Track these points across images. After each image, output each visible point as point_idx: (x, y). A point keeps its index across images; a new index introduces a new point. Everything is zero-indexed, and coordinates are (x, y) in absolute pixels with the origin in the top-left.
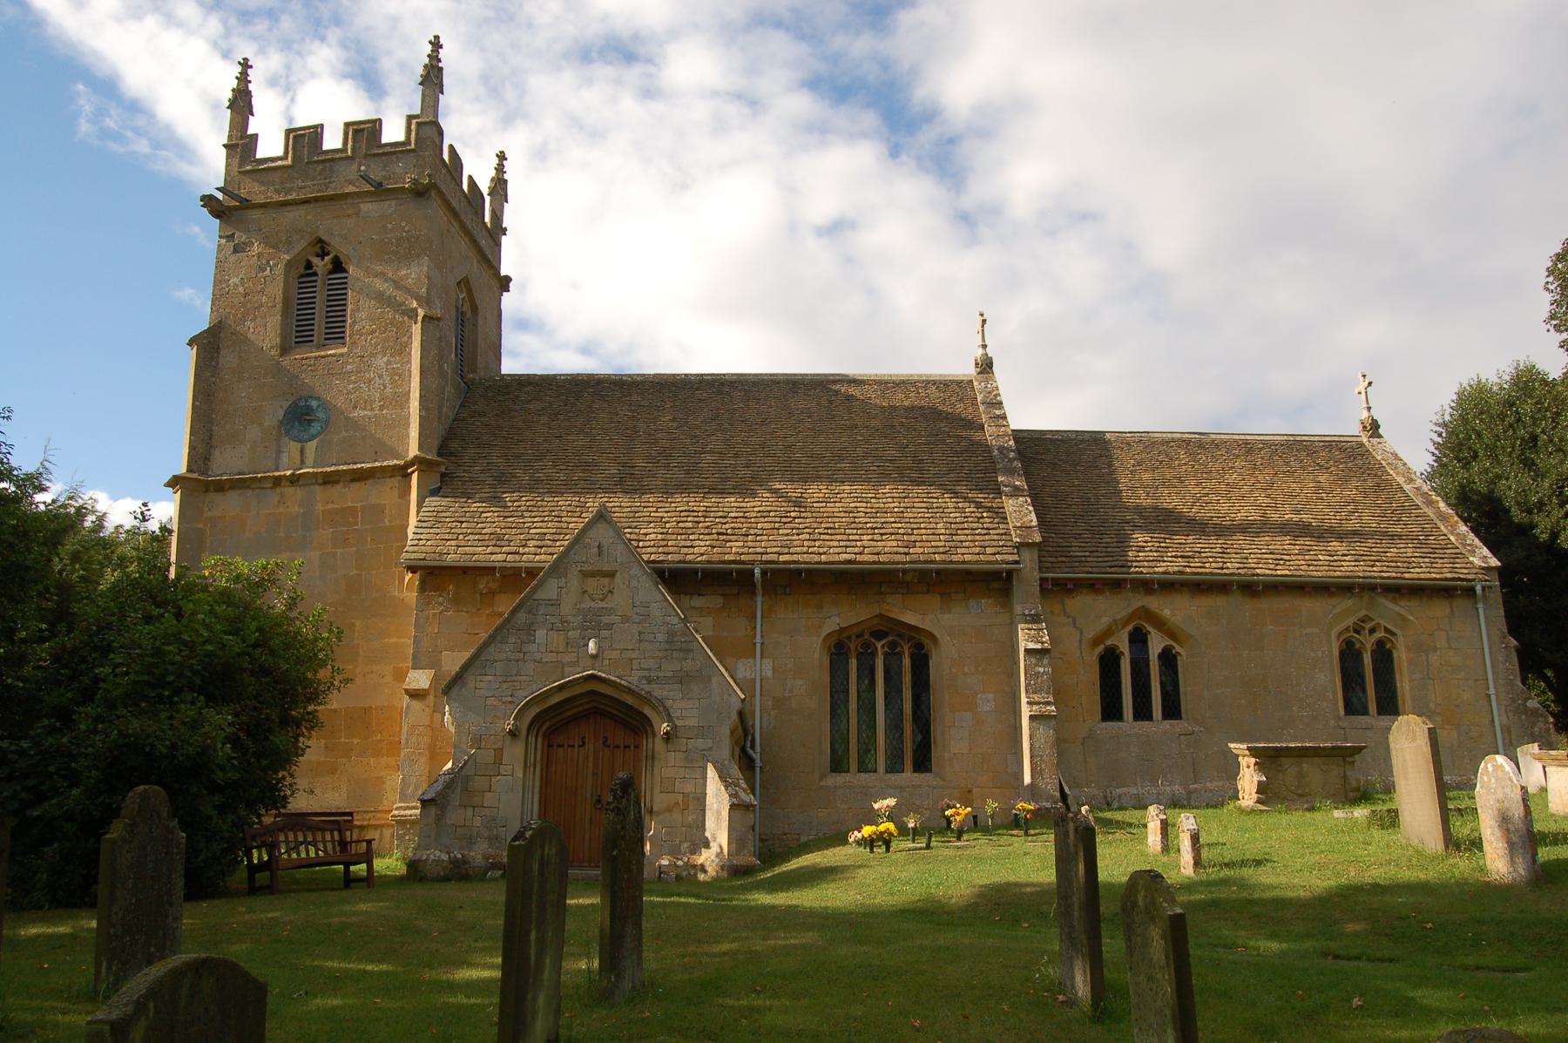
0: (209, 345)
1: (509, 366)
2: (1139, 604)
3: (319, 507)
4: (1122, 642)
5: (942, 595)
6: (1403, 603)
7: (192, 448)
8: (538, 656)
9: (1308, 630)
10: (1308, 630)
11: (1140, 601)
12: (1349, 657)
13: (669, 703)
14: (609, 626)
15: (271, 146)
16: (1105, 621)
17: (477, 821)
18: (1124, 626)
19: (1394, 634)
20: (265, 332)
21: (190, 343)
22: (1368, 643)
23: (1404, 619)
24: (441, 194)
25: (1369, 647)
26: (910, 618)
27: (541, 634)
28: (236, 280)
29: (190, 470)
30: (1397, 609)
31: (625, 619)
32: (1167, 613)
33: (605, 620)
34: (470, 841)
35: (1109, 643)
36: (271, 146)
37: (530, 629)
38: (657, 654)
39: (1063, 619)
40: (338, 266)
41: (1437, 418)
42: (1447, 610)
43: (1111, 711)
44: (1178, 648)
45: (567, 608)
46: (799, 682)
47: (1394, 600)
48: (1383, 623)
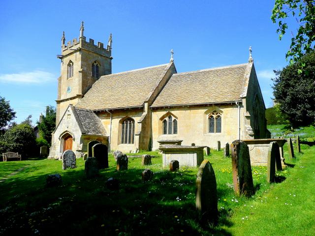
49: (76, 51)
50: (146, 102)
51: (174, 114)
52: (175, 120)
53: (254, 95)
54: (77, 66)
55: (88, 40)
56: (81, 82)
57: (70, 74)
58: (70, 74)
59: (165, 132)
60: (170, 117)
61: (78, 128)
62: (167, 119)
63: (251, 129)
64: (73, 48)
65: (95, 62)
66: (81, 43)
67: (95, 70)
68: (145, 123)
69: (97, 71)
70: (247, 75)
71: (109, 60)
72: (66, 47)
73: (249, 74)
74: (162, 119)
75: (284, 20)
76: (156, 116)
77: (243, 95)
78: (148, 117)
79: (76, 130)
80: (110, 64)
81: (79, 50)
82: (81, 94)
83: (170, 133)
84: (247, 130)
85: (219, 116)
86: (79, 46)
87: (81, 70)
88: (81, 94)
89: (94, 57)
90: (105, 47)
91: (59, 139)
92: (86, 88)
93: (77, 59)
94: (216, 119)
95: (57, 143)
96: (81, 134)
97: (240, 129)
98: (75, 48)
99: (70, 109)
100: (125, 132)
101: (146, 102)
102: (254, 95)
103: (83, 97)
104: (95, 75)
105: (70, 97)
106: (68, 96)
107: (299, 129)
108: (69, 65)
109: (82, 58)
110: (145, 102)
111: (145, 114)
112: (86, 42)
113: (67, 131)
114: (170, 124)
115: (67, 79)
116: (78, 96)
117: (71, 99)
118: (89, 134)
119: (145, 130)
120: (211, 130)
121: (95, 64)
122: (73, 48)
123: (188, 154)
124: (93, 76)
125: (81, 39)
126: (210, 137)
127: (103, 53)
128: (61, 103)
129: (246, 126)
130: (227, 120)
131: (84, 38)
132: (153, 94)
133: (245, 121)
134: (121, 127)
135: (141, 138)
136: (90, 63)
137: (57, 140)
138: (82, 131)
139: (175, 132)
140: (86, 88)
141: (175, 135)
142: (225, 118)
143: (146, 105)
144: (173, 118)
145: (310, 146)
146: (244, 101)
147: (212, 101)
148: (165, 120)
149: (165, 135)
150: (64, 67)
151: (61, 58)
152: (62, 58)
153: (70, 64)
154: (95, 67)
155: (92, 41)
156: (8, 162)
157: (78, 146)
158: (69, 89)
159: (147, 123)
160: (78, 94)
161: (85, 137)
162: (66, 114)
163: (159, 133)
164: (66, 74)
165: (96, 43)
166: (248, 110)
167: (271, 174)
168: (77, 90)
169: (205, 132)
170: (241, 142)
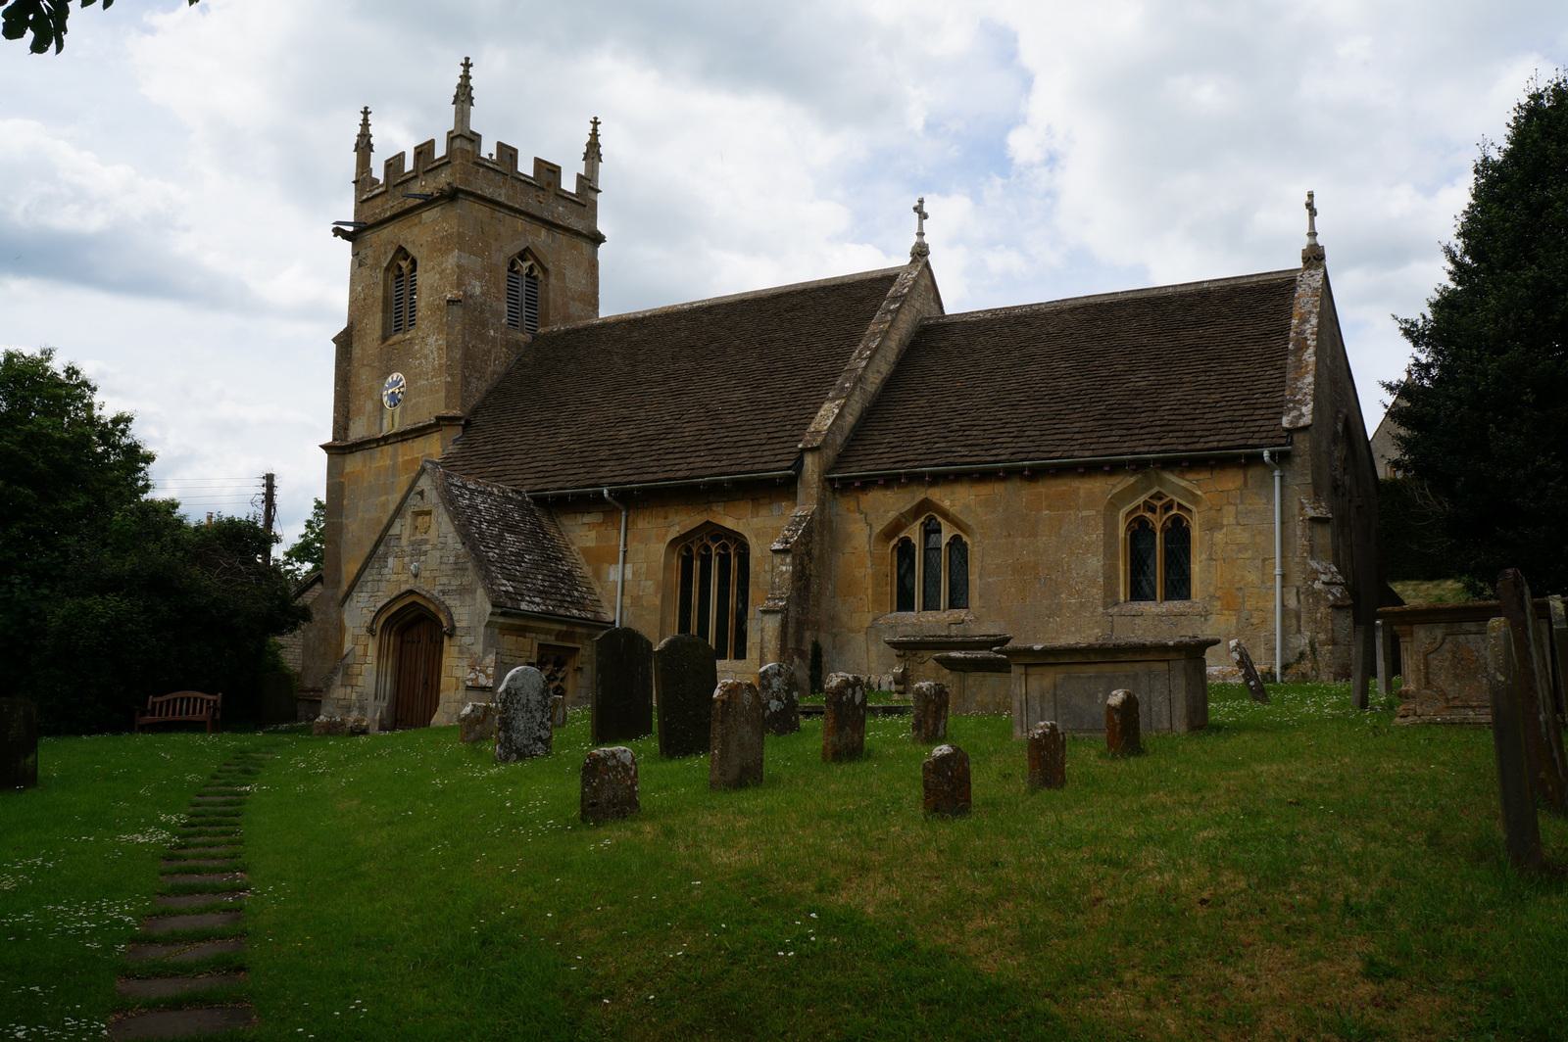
0: (345, 342)
1: (609, 308)
2: (923, 496)
3: (400, 460)
4: (915, 533)
5: (752, 500)
6: (1190, 476)
7: (336, 422)
8: (388, 577)
9: (1085, 513)
10: (1085, 513)
11: (920, 494)
12: (1140, 531)
13: (453, 610)
14: (425, 553)
15: (378, 172)
16: (892, 515)
17: (354, 697)
18: (916, 518)
19: (1189, 511)
20: (374, 324)
21: (334, 340)
22: (1157, 521)
23: (1194, 495)
24: (462, 191)
25: (1158, 526)
26: (729, 523)
27: (390, 560)
28: (360, 288)
29: (335, 439)
30: (1183, 483)
31: (434, 547)
32: (946, 504)
33: (424, 548)
34: (348, 709)
35: (902, 535)
36: (378, 172)
37: (385, 557)
38: (450, 573)
39: (857, 516)
40: (414, 262)
41: (1455, 231)
42: (1239, 482)
43: (1138, 593)
44: (965, 538)
45: (404, 542)
46: (650, 583)
47: (1182, 474)
48: (1177, 499)
52: (956, 539)
53: (1336, 418)
59: (905, 602)
60: (931, 530)
62: (915, 533)
68: (809, 553)
71: (586, 247)
74: (890, 532)
75: (647, 923)
80: (594, 265)
83: (931, 604)
84: (1318, 585)
95: (359, 650)
96: (489, 608)
102: (1336, 418)
106: (386, 423)
111: (804, 507)
113: (411, 592)
114: (930, 551)
115: (385, 338)
117: (404, 436)
119: (807, 587)
123: (602, 233)
126: (1138, 621)
129: (1314, 564)
134: (676, 578)
136: (501, 259)
137: (356, 639)
139: (959, 598)
142: (1213, 526)
144: (947, 534)
148: (906, 542)
149: (1148, 607)
155: (508, 153)
156: (916, 609)
159: (816, 552)
167: (336, 366)
169: (1111, 598)
170: (185, 522)
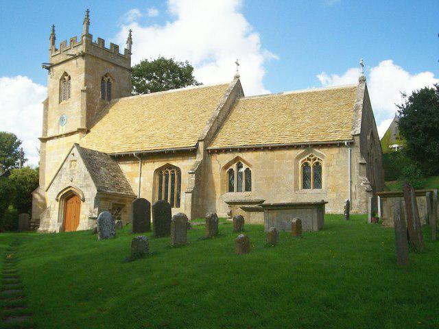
49: (75, 57)
50: (201, 141)
51: (244, 158)
52: (248, 169)
54: (78, 82)
55: (95, 40)
56: (85, 108)
57: (64, 94)
58: (64, 94)
61: (90, 181)
63: (368, 182)
64: (70, 52)
65: (106, 76)
66: (84, 44)
67: (106, 90)
69: (109, 89)
70: (359, 101)
72: (56, 50)
73: (362, 101)
74: (226, 167)
76: (218, 164)
77: (355, 132)
78: (205, 164)
79: (87, 186)
81: (83, 55)
82: (84, 127)
85: (317, 163)
86: (82, 49)
87: (85, 88)
88: (84, 127)
89: (104, 68)
90: (122, 52)
91: (57, 200)
92: (93, 115)
93: (77, 72)
94: (314, 167)
96: (96, 192)
97: (351, 182)
98: (74, 52)
99: (75, 151)
100: (163, 189)
101: (201, 141)
103: (88, 131)
104: (106, 97)
105: (66, 132)
107: (95, 207)
108: (62, 79)
109: (86, 69)
110: (199, 141)
112: (92, 44)
113: (70, 187)
115: (60, 103)
116: (80, 130)
118: (109, 191)
120: (305, 186)
121: (106, 79)
122: (70, 52)
124: (103, 98)
125: (84, 38)
127: (118, 61)
128: (48, 142)
130: (331, 169)
131: (89, 36)
132: (211, 130)
133: (360, 170)
135: (195, 196)
136: (99, 76)
138: (97, 186)
139: (248, 188)
140: (93, 115)
141: (248, 193)
142: (328, 166)
143: (201, 145)
145: (340, 76)
146: (357, 140)
147: (307, 140)
150: (53, 81)
151: (48, 68)
152: (49, 67)
153: (65, 78)
154: (106, 84)
155: (102, 41)
157: (91, 211)
158: (62, 119)
160: (80, 127)
161: (102, 197)
162: (69, 160)
163: (222, 189)
164: (58, 95)
165: (107, 46)
166: (362, 153)
168: (77, 122)
